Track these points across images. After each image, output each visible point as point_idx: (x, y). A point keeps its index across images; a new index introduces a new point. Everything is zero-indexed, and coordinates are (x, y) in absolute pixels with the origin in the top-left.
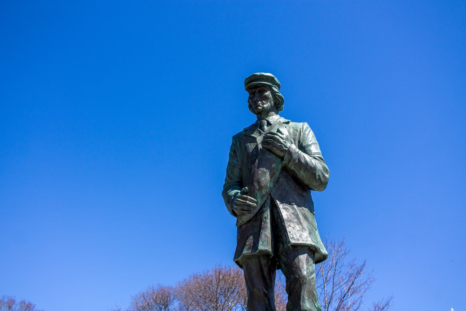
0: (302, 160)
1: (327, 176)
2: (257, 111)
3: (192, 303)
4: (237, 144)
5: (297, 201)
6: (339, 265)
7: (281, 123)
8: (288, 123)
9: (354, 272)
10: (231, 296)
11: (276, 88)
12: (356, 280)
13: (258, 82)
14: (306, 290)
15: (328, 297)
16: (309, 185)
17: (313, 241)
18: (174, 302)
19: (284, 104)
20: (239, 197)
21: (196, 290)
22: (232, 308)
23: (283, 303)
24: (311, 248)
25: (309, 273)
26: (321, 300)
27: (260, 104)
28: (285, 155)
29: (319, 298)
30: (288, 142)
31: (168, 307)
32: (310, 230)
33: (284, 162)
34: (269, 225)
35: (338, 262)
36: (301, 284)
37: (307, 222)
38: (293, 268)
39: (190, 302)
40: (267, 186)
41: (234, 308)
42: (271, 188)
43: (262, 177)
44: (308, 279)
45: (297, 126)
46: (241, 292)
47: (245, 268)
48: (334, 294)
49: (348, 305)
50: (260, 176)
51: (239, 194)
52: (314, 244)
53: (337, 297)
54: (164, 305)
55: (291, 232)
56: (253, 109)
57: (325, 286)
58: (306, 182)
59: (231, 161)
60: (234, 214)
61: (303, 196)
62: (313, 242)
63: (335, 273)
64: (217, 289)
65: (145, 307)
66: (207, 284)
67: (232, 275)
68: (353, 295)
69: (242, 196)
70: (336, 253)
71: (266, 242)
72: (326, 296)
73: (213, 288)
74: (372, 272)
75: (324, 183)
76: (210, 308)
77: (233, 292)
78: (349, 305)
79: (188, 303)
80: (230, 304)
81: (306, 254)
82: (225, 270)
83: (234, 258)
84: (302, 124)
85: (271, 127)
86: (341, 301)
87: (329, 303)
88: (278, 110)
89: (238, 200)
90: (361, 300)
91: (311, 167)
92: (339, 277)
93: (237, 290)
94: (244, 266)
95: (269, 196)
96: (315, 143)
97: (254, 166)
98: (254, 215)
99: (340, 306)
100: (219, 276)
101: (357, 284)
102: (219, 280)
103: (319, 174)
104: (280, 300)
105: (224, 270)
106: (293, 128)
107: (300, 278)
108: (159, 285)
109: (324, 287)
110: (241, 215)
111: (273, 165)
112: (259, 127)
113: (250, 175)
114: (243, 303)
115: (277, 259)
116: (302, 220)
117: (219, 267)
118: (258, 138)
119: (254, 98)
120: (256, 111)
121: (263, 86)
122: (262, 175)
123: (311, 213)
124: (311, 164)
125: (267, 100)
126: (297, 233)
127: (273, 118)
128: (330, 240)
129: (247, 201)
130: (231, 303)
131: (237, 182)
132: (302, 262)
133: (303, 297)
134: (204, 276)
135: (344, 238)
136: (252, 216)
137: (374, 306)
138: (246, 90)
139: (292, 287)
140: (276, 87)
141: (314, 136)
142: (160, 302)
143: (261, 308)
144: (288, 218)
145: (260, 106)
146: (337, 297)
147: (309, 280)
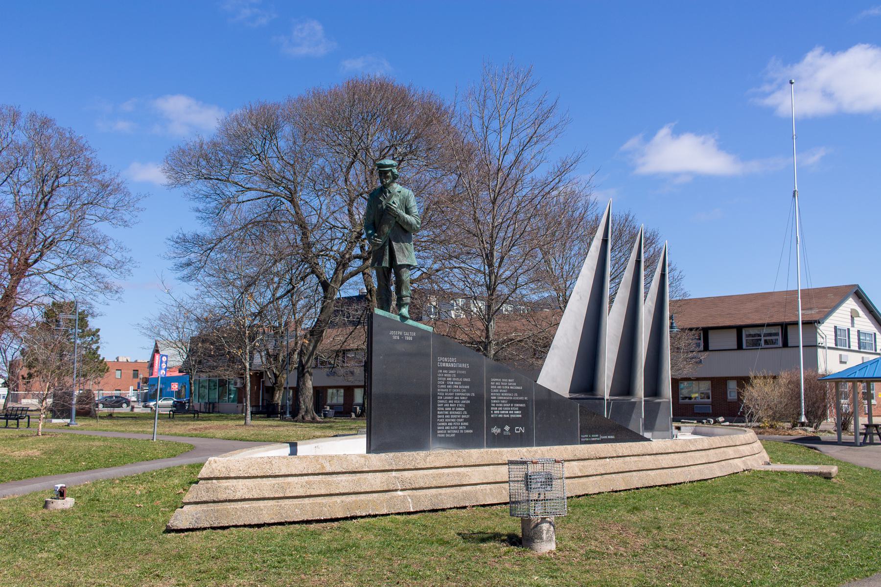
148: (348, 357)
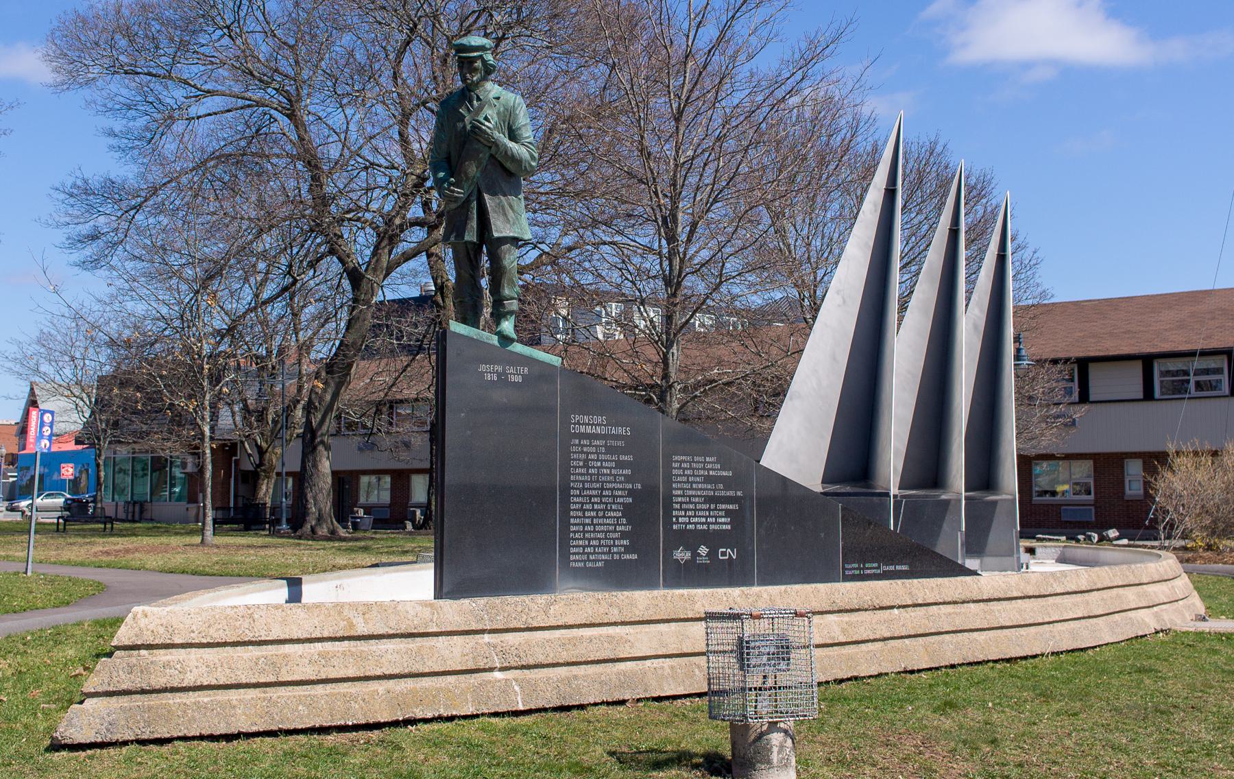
148: (399, 414)
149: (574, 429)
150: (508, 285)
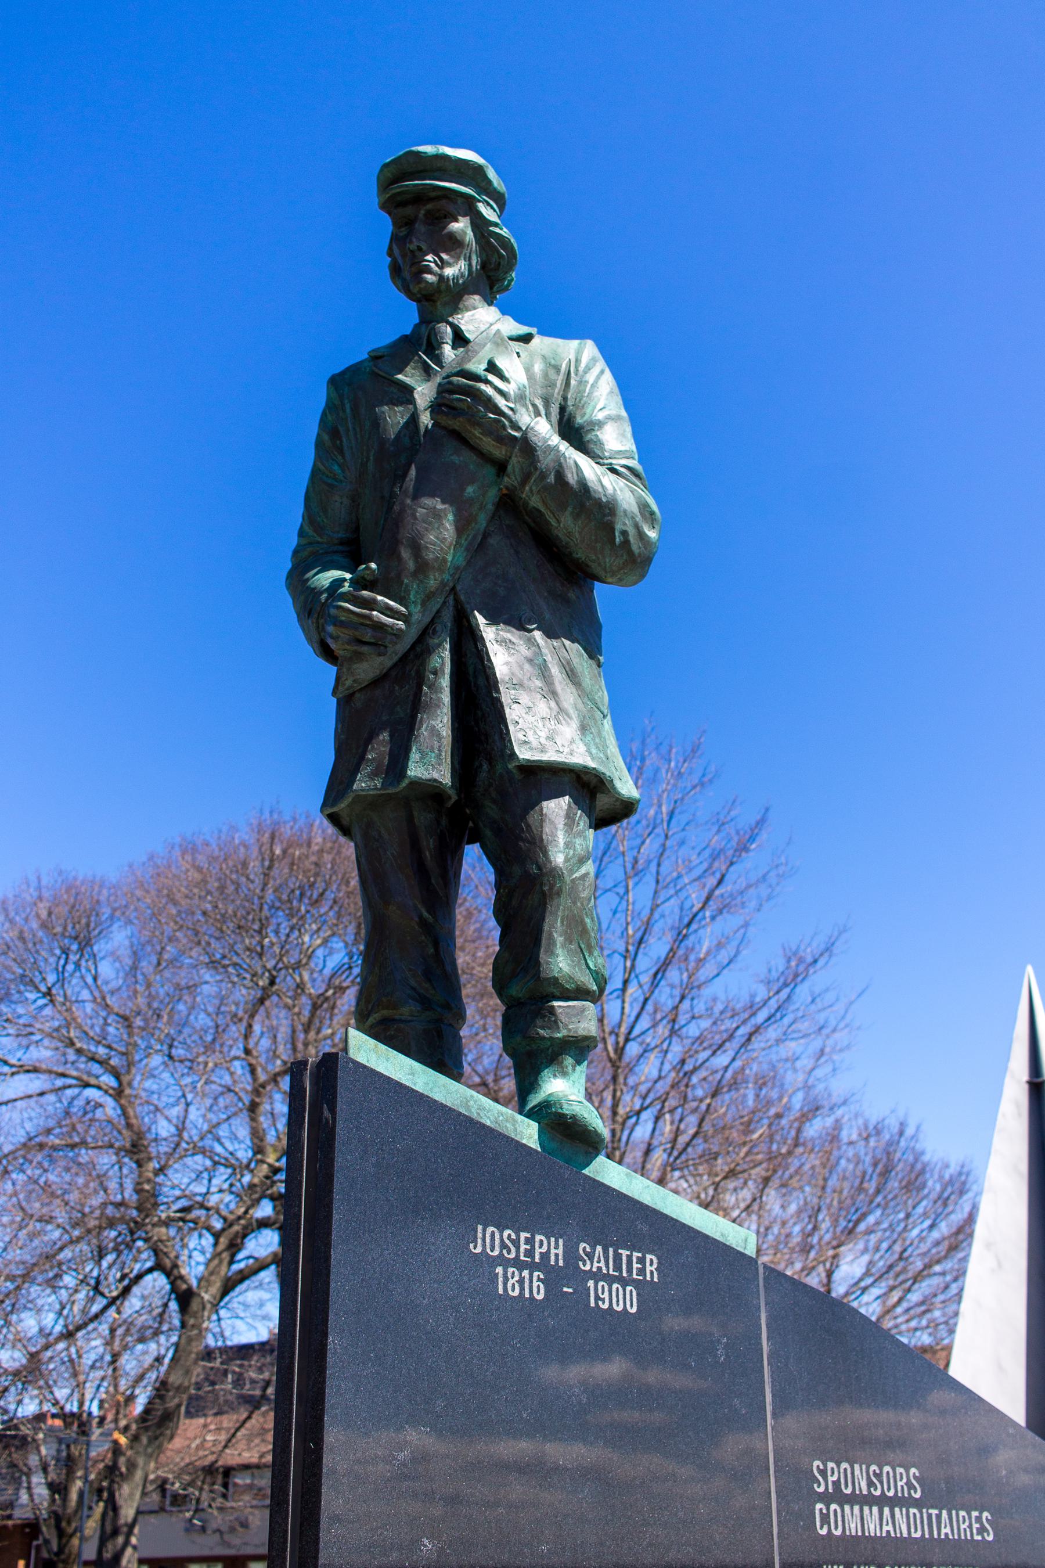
0: (569, 476)
1: (652, 534)
2: (421, 289)
3: (178, 934)
4: (343, 405)
5: (544, 619)
6: (680, 819)
7: (502, 339)
8: (526, 339)
9: (729, 846)
10: (313, 916)
11: (492, 208)
12: (732, 869)
13: (428, 182)
14: (560, 914)
15: (639, 923)
16: (590, 564)
17: (590, 753)
18: (111, 932)
19: (518, 267)
20: (344, 597)
21: (191, 891)
22: (313, 952)
23: (488, 938)
24: (585, 778)
25: (575, 860)
26: (614, 933)
27: (433, 265)
28: (511, 454)
29: (608, 929)
30: (523, 410)
31: (91, 946)
32: (584, 717)
33: (506, 479)
34: (446, 698)
35: (677, 811)
36: (544, 894)
37: (574, 690)
38: (521, 844)
39: (168, 930)
40: (445, 560)
41: (320, 953)
42: (457, 568)
43: (427, 529)
44: (568, 879)
45: (560, 350)
46: (347, 901)
47: (358, 838)
48: (656, 915)
49: (701, 948)
50: (420, 527)
51: (347, 584)
52: (594, 766)
53: (666, 923)
54: (76, 938)
55: (520, 721)
56: (404, 280)
57: (630, 887)
58: (581, 554)
59: (322, 468)
60: (327, 653)
61: (567, 601)
62: (593, 759)
63: (664, 845)
64: (263, 890)
65: (11, 944)
66: (228, 872)
67: (317, 844)
68: (719, 918)
69: (355, 593)
70: (672, 781)
71: (433, 755)
72: (633, 919)
73: (251, 886)
74: (788, 844)
75: (639, 560)
76: (239, 951)
77: (317, 901)
78: (704, 949)
79: (162, 934)
80: (306, 939)
81: (567, 798)
82: (292, 828)
83: (324, 805)
84: (575, 343)
85: (467, 353)
86: (680, 937)
87: (640, 942)
88: (495, 289)
89: (341, 607)
90: (744, 934)
91: (598, 503)
92: (677, 858)
93: (333, 896)
94: (356, 830)
95: (452, 597)
96: (617, 418)
97: (401, 488)
98: (396, 658)
99: (675, 954)
100: (271, 846)
101: (735, 882)
102: (272, 861)
103: (624, 528)
104: (478, 930)
105: (288, 826)
106: (544, 357)
107: (542, 875)
108: (60, 873)
109: (627, 891)
110: (351, 658)
111: (470, 490)
112: (424, 347)
113: (386, 520)
114: (350, 938)
115: (468, 811)
116: (560, 683)
117: (271, 816)
118: (419, 389)
119: (411, 242)
120: (415, 289)
121: (445, 197)
122: (430, 523)
123: (590, 661)
124: (600, 490)
125: (458, 251)
126: (540, 724)
127: (476, 317)
128: (657, 738)
129: (375, 613)
130: (311, 937)
131: (342, 543)
132: (552, 822)
133: (550, 935)
134: (218, 845)
135: (704, 732)
136: (389, 663)
137: (785, 956)
138: (385, 206)
139: (514, 902)
140: (492, 202)
141: (617, 390)
142: (65, 928)
143: (410, 970)
144: (513, 674)
145: (429, 271)
146: (666, 923)
147: (573, 881)
148: (235, 1485)
149: (825, 1519)
150: (569, 940)
